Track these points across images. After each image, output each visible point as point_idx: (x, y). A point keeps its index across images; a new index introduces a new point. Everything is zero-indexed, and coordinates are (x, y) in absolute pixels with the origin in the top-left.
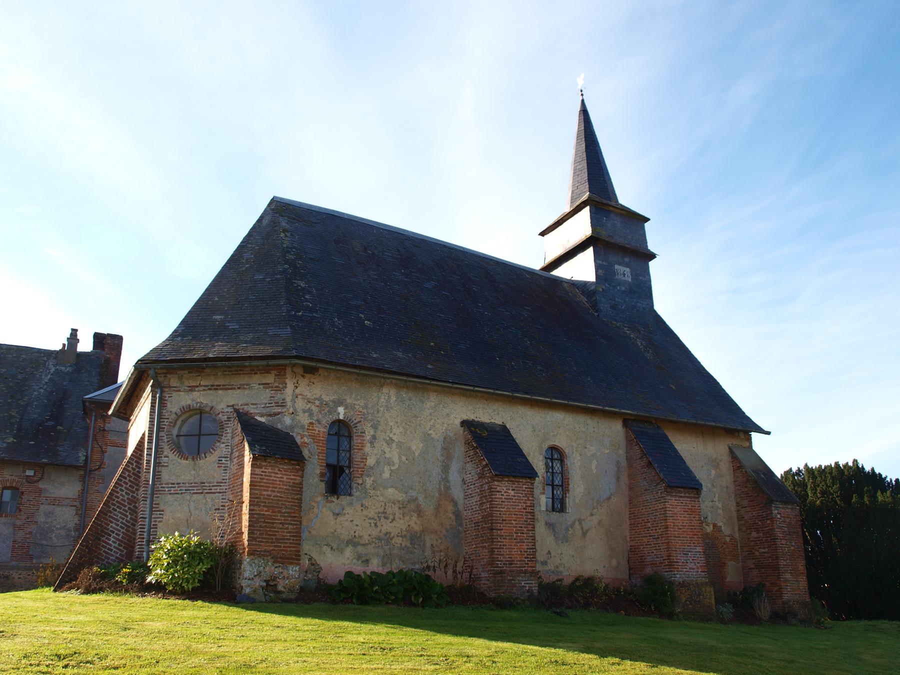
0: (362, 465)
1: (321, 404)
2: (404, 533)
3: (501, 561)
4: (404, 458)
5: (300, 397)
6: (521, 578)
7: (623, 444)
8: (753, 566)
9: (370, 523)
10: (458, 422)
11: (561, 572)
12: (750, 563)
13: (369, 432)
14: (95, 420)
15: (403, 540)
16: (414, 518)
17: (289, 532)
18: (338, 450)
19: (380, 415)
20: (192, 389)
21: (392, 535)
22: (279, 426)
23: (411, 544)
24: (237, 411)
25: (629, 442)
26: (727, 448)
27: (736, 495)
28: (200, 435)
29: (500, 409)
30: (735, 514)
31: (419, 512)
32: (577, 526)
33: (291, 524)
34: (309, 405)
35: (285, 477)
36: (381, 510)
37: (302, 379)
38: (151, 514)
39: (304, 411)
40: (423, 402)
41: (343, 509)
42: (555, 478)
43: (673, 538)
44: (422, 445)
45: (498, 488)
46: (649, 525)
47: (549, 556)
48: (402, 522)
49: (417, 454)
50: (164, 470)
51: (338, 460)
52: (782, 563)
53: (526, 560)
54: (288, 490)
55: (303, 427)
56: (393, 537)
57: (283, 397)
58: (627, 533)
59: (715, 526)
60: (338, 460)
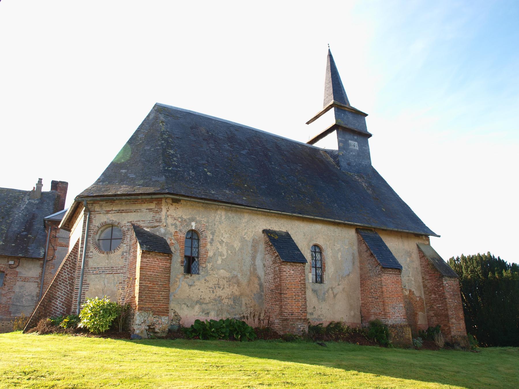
0: (205, 256)
1: (182, 220)
2: (229, 296)
3: (287, 313)
4: (229, 252)
5: (169, 216)
6: (298, 323)
8: (433, 315)
9: (210, 291)
10: (261, 231)
12: (431, 313)
13: (209, 237)
15: (229, 301)
16: (236, 287)
17: (163, 296)
18: (192, 247)
19: (216, 227)
20: (108, 212)
21: (223, 298)
22: (158, 234)
23: (234, 303)
25: (359, 242)
26: (416, 245)
27: (422, 273)
28: (111, 239)
29: (285, 223)
30: (421, 284)
31: (238, 284)
32: (330, 291)
33: (164, 291)
34: (175, 221)
35: (161, 263)
36: (216, 283)
38: (82, 286)
39: (172, 225)
40: (240, 219)
41: (194, 282)
42: (317, 263)
43: (386, 298)
44: (240, 244)
45: (284, 270)
46: (372, 291)
47: (314, 309)
48: (228, 290)
49: (237, 250)
50: (90, 260)
51: (191, 253)
53: (301, 312)
54: (162, 271)
55: (171, 234)
56: (223, 299)
58: (360, 296)
59: (410, 291)
60: (191, 253)
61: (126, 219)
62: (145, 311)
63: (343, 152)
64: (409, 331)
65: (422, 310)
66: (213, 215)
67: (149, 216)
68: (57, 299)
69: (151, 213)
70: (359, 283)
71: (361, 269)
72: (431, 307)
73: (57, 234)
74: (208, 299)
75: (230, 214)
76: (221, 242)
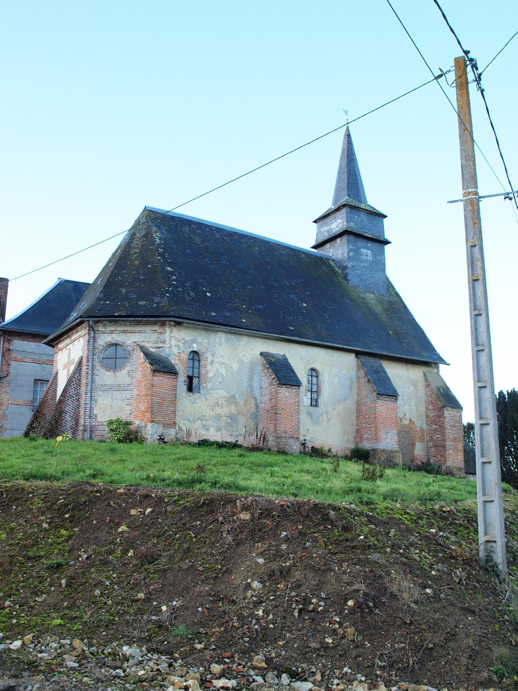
0: (206, 376)
1: (185, 342)
2: (228, 415)
4: (228, 373)
5: (173, 338)
7: (355, 369)
8: (432, 446)
10: (258, 353)
11: (314, 441)
12: (431, 444)
13: (210, 358)
14: (3, 342)
16: (233, 407)
18: (193, 368)
19: (216, 348)
20: (112, 332)
24: (138, 345)
25: (358, 367)
26: (422, 373)
27: (426, 402)
28: (116, 358)
30: (424, 414)
31: (236, 404)
32: (325, 415)
34: (178, 342)
36: (216, 402)
37: (174, 328)
38: (91, 402)
39: (176, 346)
40: (239, 341)
41: (196, 400)
45: (280, 391)
46: (367, 416)
48: (227, 408)
50: (97, 377)
51: (193, 373)
52: (448, 443)
55: (175, 355)
57: (164, 338)
58: (355, 422)
59: (410, 420)
60: (193, 373)
61: (131, 339)
62: (157, 423)
63: (353, 262)
64: (399, 456)
65: (422, 440)
66: (214, 336)
67: (154, 337)
68: (66, 413)
69: (155, 334)
70: (355, 409)
71: (358, 395)
72: (431, 437)
73: (11, 346)
74: (208, 416)
75: (229, 336)
76: (221, 364)
